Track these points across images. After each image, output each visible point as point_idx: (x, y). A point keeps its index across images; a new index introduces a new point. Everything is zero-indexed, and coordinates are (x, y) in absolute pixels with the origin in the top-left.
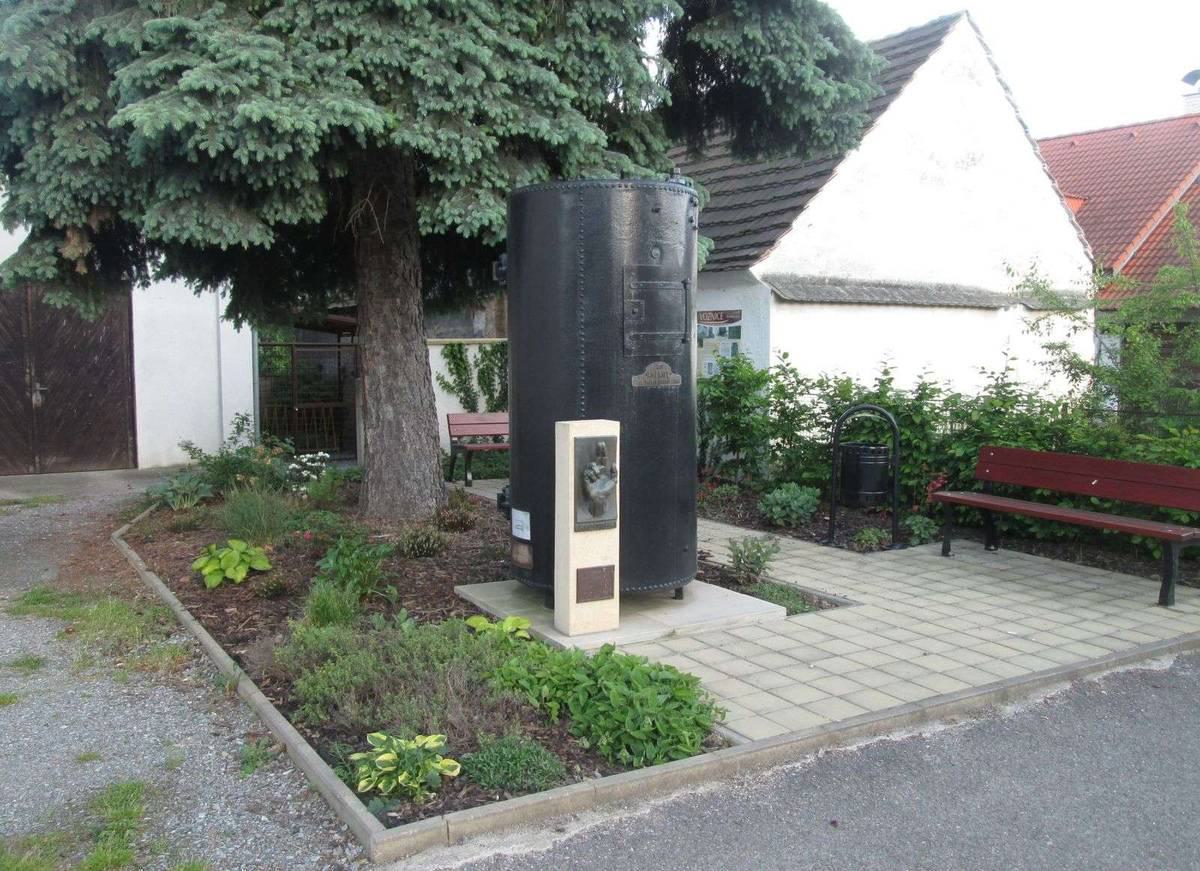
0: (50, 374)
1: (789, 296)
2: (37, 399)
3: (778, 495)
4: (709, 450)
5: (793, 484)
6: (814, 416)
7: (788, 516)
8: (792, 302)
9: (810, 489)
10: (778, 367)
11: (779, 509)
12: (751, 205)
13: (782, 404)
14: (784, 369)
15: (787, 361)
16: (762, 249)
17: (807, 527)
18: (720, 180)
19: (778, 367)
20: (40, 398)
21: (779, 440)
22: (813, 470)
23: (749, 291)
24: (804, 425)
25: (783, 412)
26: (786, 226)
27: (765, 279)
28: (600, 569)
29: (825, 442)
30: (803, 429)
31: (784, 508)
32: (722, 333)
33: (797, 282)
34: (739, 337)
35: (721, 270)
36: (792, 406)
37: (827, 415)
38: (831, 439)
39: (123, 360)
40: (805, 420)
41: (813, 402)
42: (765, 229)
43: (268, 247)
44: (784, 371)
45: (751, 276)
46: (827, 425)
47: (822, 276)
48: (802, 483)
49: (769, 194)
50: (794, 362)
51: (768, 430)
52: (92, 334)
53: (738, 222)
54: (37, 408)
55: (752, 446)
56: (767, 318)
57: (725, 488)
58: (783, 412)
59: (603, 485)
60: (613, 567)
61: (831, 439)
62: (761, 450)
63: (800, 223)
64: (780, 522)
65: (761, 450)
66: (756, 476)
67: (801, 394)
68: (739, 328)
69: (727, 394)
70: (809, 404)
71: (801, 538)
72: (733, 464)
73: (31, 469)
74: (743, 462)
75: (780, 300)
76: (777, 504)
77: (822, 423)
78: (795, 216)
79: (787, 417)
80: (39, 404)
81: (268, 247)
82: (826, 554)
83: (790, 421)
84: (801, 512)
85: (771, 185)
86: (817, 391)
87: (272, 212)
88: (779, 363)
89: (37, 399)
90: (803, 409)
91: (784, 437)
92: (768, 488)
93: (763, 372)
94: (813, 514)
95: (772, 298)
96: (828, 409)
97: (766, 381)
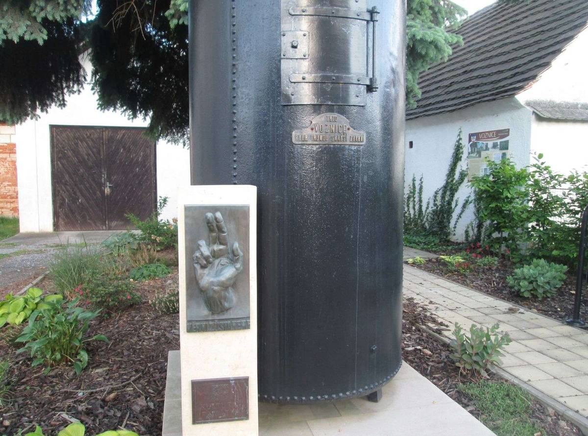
0: (114, 178)
1: (547, 115)
2: (107, 191)
3: (527, 270)
4: (483, 230)
5: (542, 261)
6: (565, 204)
7: (534, 289)
8: (549, 120)
9: (557, 266)
10: (535, 166)
11: (526, 283)
12: (521, 58)
13: (537, 195)
14: (539, 167)
15: (541, 160)
16: (526, 82)
17: (553, 299)
18: (500, 47)
19: (535, 166)
20: (109, 190)
21: (534, 224)
22: (561, 249)
23: (516, 114)
24: (556, 212)
25: (538, 201)
26: (547, 65)
27: (528, 104)
28: (226, 381)
29: (574, 226)
30: (555, 215)
31: (531, 283)
32: (495, 146)
33: (554, 107)
34: (507, 149)
35: (494, 99)
36: (545, 196)
37: (576, 204)
38: (580, 224)
39: (151, 171)
40: (556, 208)
41: (564, 194)
42: (530, 70)
43: (41, 42)
44: (539, 169)
45: (517, 102)
46: (577, 213)
47: (575, 102)
48: (550, 259)
49: (535, 48)
50: (547, 161)
51: (524, 216)
52: (135, 157)
53: (510, 70)
54: (107, 195)
55: (512, 228)
56: (529, 133)
57: (488, 259)
58: (538, 201)
59: (218, 273)
60: (245, 381)
61: (580, 224)
62: (519, 230)
63: (558, 62)
64: (526, 295)
65: (519, 230)
66: (516, 250)
67: (554, 187)
68: (507, 142)
69: (493, 187)
70: (560, 195)
71: (545, 313)
72: (499, 241)
73: (104, 228)
74: (505, 239)
75: (540, 119)
76: (525, 279)
77: (571, 211)
78: (553, 58)
79: (541, 205)
80: (109, 193)
81: (41, 42)
82: (569, 337)
83: (544, 209)
84: (547, 287)
85: (536, 42)
86: (568, 185)
87: (37, 10)
88: (535, 162)
89: (107, 191)
90: (556, 199)
91: (538, 221)
92: (524, 261)
93: (523, 171)
94: (559, 289)
95: (533, 117)
96: (577, 200)
97: (524, 178)
